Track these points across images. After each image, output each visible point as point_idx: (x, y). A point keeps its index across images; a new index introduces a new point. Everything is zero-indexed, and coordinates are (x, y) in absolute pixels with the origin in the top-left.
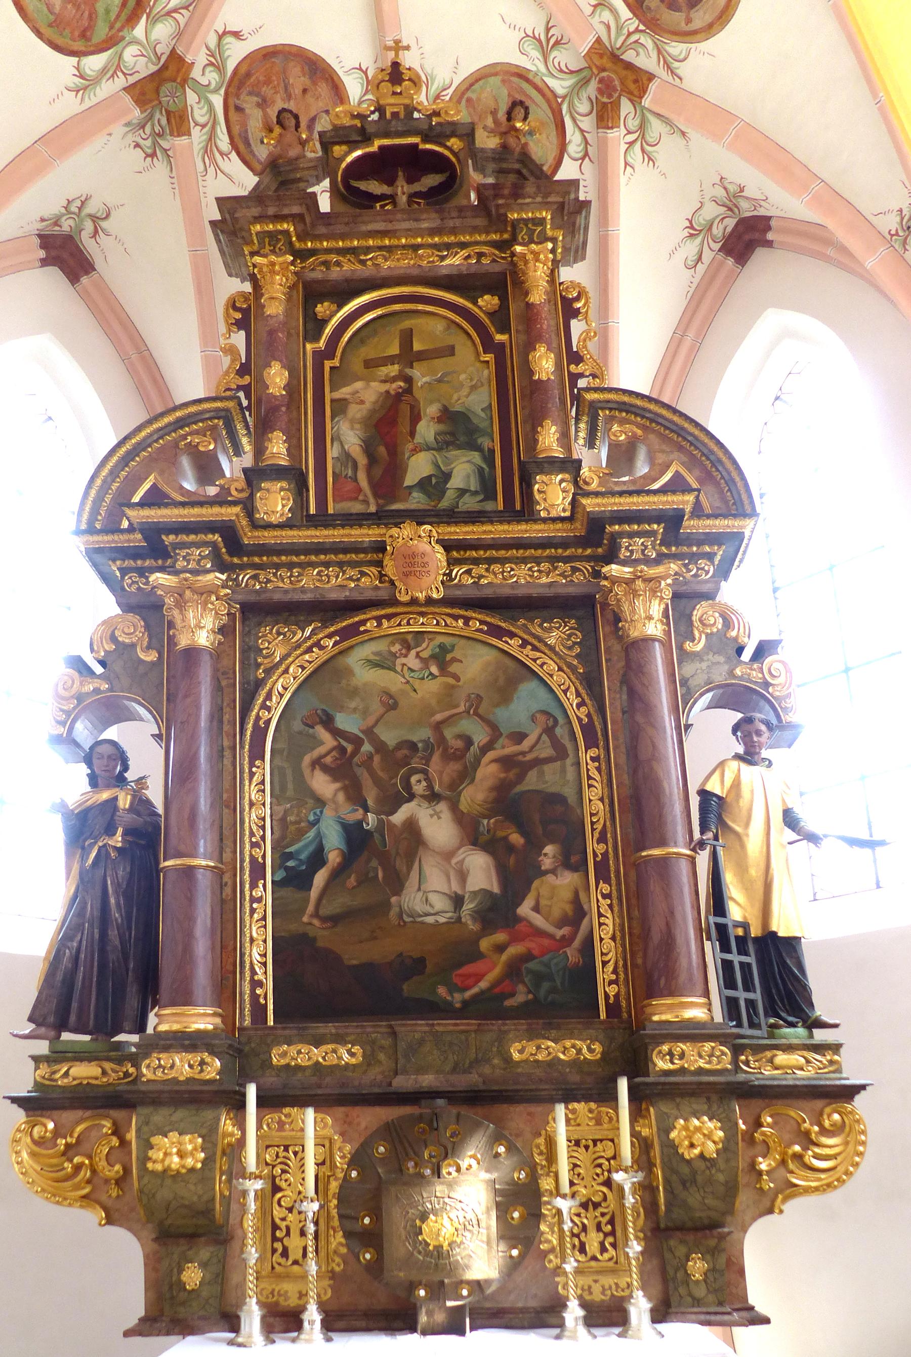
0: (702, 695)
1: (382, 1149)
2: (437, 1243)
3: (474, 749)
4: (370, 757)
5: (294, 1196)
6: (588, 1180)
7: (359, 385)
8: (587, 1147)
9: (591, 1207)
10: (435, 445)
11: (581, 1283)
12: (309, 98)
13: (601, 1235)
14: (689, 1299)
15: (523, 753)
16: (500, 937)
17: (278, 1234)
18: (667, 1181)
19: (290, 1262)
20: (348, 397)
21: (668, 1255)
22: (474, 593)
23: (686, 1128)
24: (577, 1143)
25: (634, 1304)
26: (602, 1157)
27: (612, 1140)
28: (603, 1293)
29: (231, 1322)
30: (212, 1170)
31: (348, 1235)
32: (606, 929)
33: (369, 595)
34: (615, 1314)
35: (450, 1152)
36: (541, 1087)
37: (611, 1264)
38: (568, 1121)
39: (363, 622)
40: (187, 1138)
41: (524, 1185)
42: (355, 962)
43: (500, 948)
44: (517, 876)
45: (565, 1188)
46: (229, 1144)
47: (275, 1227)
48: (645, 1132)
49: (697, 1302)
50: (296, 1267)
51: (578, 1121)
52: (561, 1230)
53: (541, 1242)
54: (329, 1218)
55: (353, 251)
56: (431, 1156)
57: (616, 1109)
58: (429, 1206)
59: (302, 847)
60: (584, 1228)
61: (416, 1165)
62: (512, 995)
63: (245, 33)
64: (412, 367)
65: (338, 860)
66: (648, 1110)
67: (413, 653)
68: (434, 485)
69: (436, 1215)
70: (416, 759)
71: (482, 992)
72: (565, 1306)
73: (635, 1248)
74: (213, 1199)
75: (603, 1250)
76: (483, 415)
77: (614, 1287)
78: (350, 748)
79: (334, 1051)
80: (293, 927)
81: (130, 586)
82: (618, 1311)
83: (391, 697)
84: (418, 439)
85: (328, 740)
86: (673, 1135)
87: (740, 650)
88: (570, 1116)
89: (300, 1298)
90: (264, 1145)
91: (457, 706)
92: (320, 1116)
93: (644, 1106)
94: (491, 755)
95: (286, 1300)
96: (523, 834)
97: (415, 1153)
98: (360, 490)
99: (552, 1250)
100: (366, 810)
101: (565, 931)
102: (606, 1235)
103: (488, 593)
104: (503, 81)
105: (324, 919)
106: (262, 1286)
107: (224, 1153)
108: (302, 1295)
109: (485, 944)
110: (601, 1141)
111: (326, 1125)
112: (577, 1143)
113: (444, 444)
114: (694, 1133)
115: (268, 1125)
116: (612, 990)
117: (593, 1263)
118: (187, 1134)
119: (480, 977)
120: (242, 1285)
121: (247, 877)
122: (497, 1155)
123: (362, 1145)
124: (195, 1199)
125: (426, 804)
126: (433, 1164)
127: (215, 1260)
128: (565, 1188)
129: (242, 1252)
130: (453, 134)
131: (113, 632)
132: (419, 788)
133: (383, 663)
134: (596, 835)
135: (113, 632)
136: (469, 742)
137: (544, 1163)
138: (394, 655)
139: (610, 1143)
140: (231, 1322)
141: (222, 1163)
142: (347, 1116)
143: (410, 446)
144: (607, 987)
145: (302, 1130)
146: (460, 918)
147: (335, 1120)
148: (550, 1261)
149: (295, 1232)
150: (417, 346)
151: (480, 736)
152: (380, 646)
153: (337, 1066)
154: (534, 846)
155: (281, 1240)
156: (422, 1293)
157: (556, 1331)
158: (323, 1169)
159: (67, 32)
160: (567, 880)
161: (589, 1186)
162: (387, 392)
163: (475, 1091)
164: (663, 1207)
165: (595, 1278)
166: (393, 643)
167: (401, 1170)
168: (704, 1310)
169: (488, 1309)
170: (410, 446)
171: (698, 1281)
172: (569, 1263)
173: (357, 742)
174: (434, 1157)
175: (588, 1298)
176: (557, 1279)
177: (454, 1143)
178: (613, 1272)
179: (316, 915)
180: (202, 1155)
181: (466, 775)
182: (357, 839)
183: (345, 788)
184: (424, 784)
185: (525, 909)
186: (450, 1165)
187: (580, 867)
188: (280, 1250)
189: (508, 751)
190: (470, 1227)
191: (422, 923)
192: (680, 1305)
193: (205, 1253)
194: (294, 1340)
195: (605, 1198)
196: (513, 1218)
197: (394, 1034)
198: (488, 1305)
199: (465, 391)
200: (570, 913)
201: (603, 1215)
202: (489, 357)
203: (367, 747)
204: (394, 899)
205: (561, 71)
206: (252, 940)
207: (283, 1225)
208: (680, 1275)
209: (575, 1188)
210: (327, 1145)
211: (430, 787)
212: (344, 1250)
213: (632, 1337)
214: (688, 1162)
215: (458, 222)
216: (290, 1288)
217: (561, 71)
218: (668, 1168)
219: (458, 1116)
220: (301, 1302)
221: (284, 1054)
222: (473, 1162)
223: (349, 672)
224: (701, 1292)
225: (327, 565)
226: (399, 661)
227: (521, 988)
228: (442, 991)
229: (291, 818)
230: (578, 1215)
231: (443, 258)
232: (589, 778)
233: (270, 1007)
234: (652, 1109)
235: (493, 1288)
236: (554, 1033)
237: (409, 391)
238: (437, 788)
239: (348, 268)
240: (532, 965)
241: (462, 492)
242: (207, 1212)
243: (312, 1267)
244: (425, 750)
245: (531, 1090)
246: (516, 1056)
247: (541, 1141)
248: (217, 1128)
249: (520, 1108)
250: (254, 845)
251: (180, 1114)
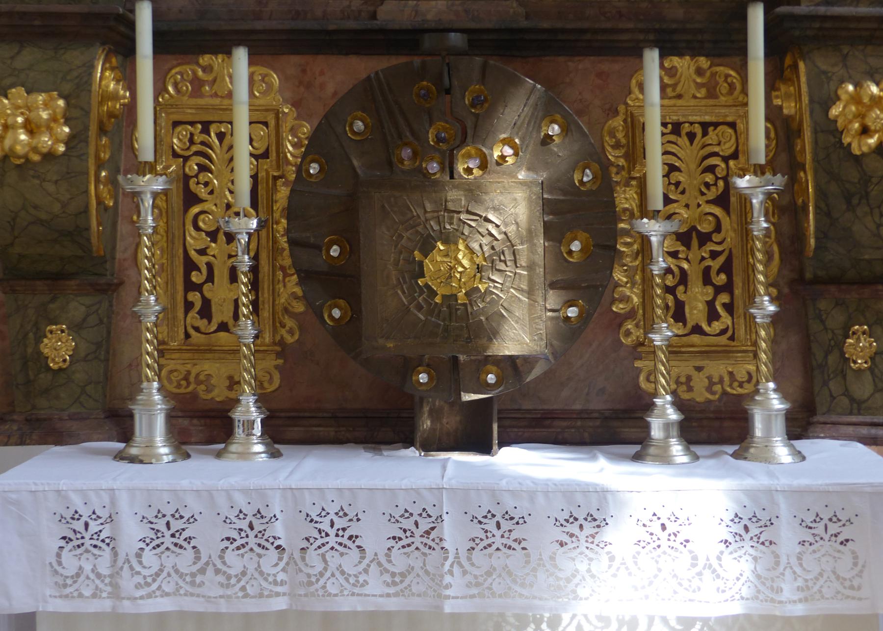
1: (359, 125)
2: (447, 292)
5: (219, 211)
6: (692, 193)
8: (691, 136)
9: (695, 243)
11: (675, 371)
13: (710, 290)
14: (845, 401)
17: (195, 277)
18: (821, 194)
19: (214, 327)
21: (815, 327)
23: (856, 99)
24: (676, 129)
25: (758, 403)
26: (715, 154)
27: (733, 125)
28: (709, 389)
29: (119, 424)
30: (83, 157)
31: (306, 276)
34: (727, 424)
35: (470, 132)
36: (621, 25)
37: (723, 340)
38: (663, 87)
40: (41, 98)
41: (590, 193)
45: (657, 203)
46: (111, 115)
47: (190, 266)
48: (789, 108)
49: (858, 406)
50: (222, 334)
51: (679, 89)
52: (647, 281)
53: (613, 301)
54: (276, 250)
56: (439, 140)
57: (743, 69)
58: (436, 228)
60: (684, 277)
61: (415, 154)
66: (795, 67)
69: (445, 242)
72: (649, 407)
73: (767, 306)
74: (86, 210)
75: (713, 316)
77: (726, 379)
82: (732, 419)
86: (835, 111)
88: (666, 80)
89: (230, 388)
90: (169, 118)
92: (260, 70)
93: (788, 61)
95: (208, 390)
97: (413, 133)
99: (631, 314)
102: (718, 290)
106: (172, 365)
107: (102, 130)
108: (234, 383)
110: (716, 125)
111: (270, 86)
112: (676, 129)
114: (870, 108)
115: (176, 85)
117: (695, 338)
118: (40, 91)
120: (136, 365)
122: (547, 140)
123: (326, 117)
124: (57, 208)
126: (442, 153)
127: (93, 320)
128: (657, 203)
129: (137, 300)
137: (622, 162)
139: (730, 131)
140: (119, 424)
141: (100, 147)
142: (304, 71)
145: (230, 95)
148: (628, 333)
155: (198, 288)
156: (423, 378)
157: (634, 449)
158: (266, 164)
161: (693, 204)
163: (511, 31)
164: (812, 242)
165: (698, 363)
167: (390, 164)
168: (868, 419)
169: (528, 411)
171: (860, 371)
172: (659, 331)
174: (443, 140)
175: (686, 396)
176: (638, 364)
177: (477, 116)
178: (724, 353)
186: (469, 156)
188: (198, 305)
190: (502, 266)
192: (829, 411)
193: (77, 308)
194: (219, 455)
195: (718, 229)
196: (570, 252)
198: (527, 405)
201: (714, 255)
206: (279, 281)
207: (201, 261)
208: (832, 359)
209: (672, 208)
210: (272, 123)
213: (756, 459)
214: (857, 160)
216: (213, 369)
218: (822, 165)
219: (484, 67)
220: (232, 395)
222: (508, 151)
224: (863, 389)
230: (674, 255)
234: (802, 65)
235: (537, 371)
242: (78, 233)
243: (247, 329)
245: (605, 31)
247: (617, 122)
248: (89, 82)
249: (586, 64)
251: (29, 56)
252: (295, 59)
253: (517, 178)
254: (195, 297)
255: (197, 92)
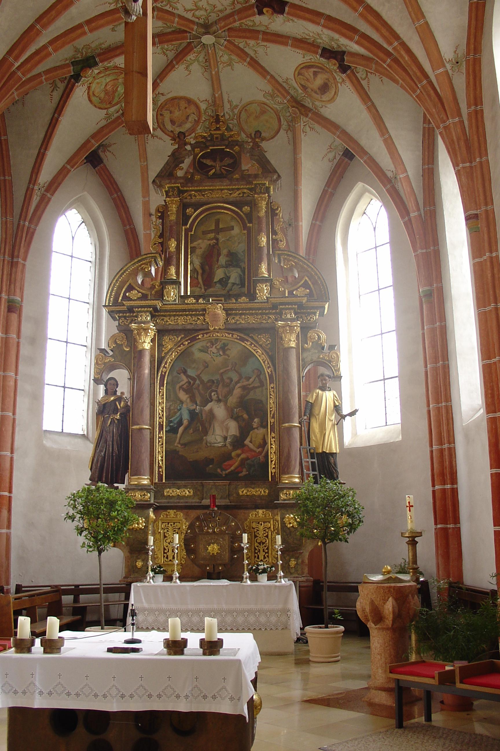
0: (309, 365)
3: (233, 382)
4: (199, 386)
7: (200, 241)
10: (225, 266)
12: (187, 110)
15: (249, 385)
16: (239, 452)
20: (196, 246)
22: (234, 326)
32: (272, 448)
33: (200, 327)
39: (198, 335)
42: (191, 460)
43: (238, 456)
44: (245, 430)
55: (200, 191)
59: (175, 419)
62: (242, 472)
63: (165, 94)
64: (218, 234)
65: (187, 423)
67: (214, 346)
68: (224, 282)
70: (214, 387)
71: (232, 471)
76: (242, 254)
78: (192, 382)
79: (184, 491)
80: (172, 447)
81: (121, 323)
83: (206, 363)
84: (219, 263)
85: (185, 379)
87: (323, 348)
91: (228, 367)
94: (239, 385)
96: (248, 415)
98: (199, 283)
100: (197, 405)
101: (260, 449)
102: (266, 553)
103: (240, 326)
104: (258, 105)
105: (182, 445)
109: (233, 454)
113: (228, 265)
116: (273, 471)
119: (231, 466)
121: (157, 430)
125: (216, 403)
130: (237, 145)
131: (115, 341)
132: (214, 397)
133: (204, 350)
134: (271, 416)
135: (115, 341)
136: (231, 380)
138: (208, 347)
143: (217, 266)
144: (271, 469)
146: (225, 445)
147: (184, 514)
149: (170, 551)
150: (221, 226)
151: (235, 378)
152: (204, 344)
153: (185, 496)
154: (251, 419)
155: (166, 553)
159: (105, 104)
160: (262, 431)
162: (210, 244)
166: (208, 343)
170: (217, 266)
173: (194, 379)
179: (179, 443)
180: (144, 524)
181: (230, 392)
182: (193, 414)
183: (190, 397)
184: (216, 395)
185: (247, 442)
187: (266, 427)
189: (245, 383)
191: (214, 446)
197: (203, 485)
199: (236, 244)
200: (262, 443)
202: (245, 232)
203: (198, 382)
204: (204, 438)
205: (279, 103)
207: (167, 548)
211: (218, 397)
212: (185, 557)
214: (289, 528)
215: (236, 183)
217: (279, 103)
221: (168, 492)
223: (193, 353)
225: (187, 315)
226: (209, 350)
227: (244, 470)
228: (219, 470)
229: (172, 408)
231: (231, 194)
232: (270, 395)
233: (164, 475)
236: (253, 486)
237: (217, 244)
238: (220, 397)
239: (199, 198)
240: (248, 462)
241: (234, 284)
244: (217, 383)
246: (241, 493)
249: (241, 511)
250: (160, 418)
252: (186, 511)
253: (321, 545)
254: (165, 555)
255: (167, 517)
